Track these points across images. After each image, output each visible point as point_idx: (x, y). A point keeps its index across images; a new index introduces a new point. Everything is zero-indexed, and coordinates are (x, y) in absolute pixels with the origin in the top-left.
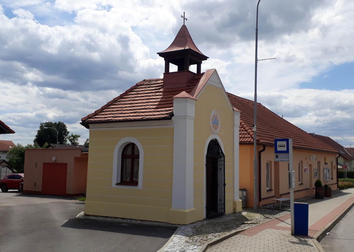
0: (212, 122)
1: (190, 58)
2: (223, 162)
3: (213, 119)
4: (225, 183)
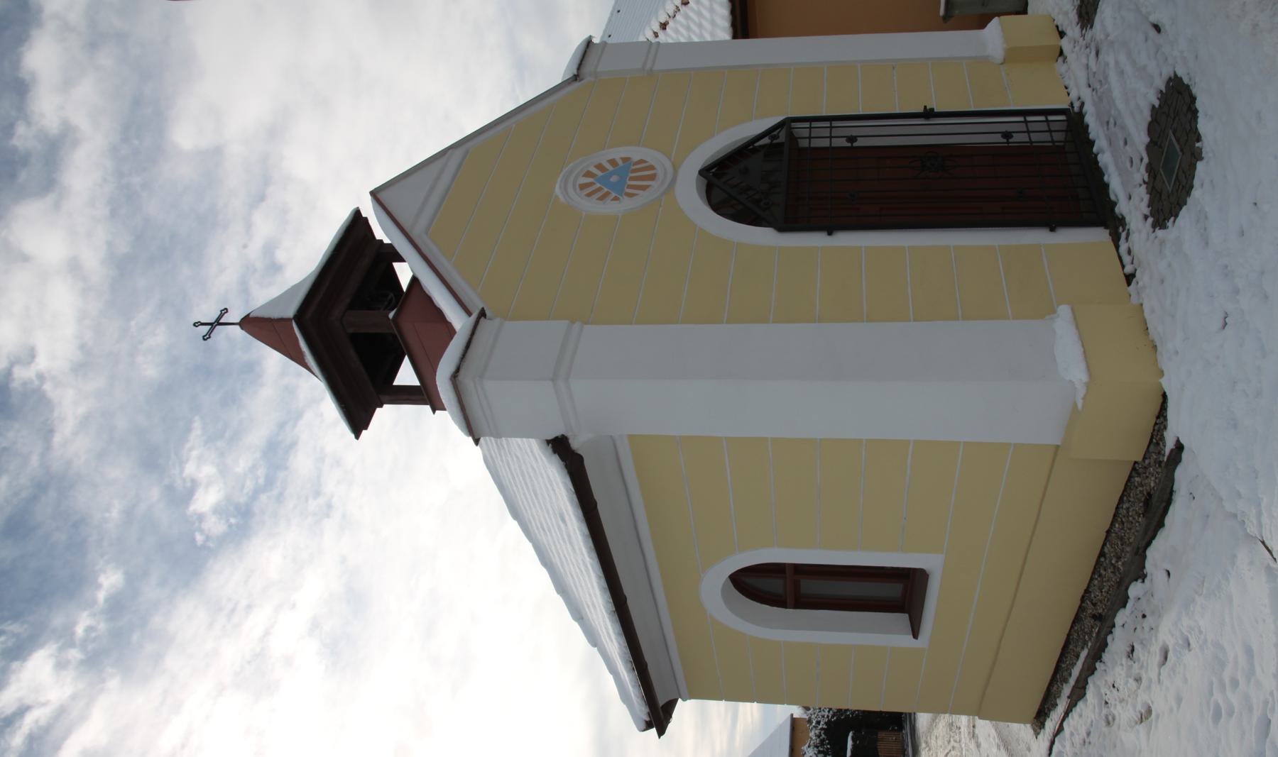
0: (616, 199)
1: (351, 307)
2: (821, 129)
3: (600, 194)
4: (921, 110)
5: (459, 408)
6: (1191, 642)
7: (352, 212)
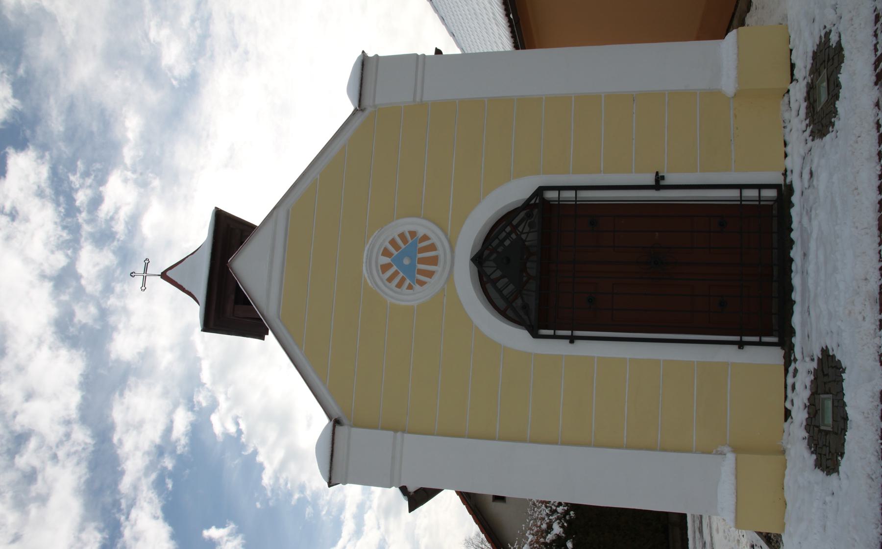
0: (410, 287)
5: (330, 455)
6: (797, 387)
7: (213, 213)
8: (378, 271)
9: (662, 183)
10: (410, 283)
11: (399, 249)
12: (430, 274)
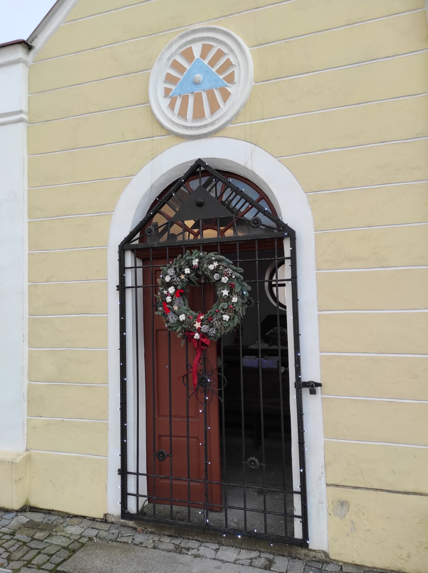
0: (167, 92)
8: (181, 47)
9: (306, 391)
10: (172, 90)
11: (179, 80)
12: (183, 114)
